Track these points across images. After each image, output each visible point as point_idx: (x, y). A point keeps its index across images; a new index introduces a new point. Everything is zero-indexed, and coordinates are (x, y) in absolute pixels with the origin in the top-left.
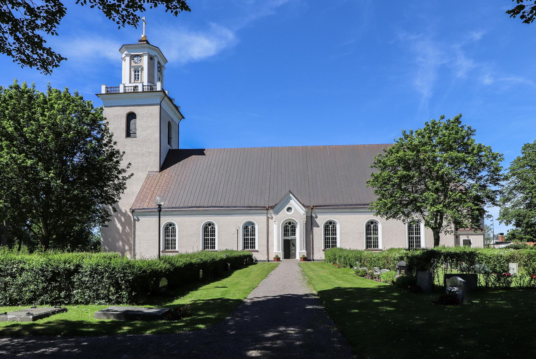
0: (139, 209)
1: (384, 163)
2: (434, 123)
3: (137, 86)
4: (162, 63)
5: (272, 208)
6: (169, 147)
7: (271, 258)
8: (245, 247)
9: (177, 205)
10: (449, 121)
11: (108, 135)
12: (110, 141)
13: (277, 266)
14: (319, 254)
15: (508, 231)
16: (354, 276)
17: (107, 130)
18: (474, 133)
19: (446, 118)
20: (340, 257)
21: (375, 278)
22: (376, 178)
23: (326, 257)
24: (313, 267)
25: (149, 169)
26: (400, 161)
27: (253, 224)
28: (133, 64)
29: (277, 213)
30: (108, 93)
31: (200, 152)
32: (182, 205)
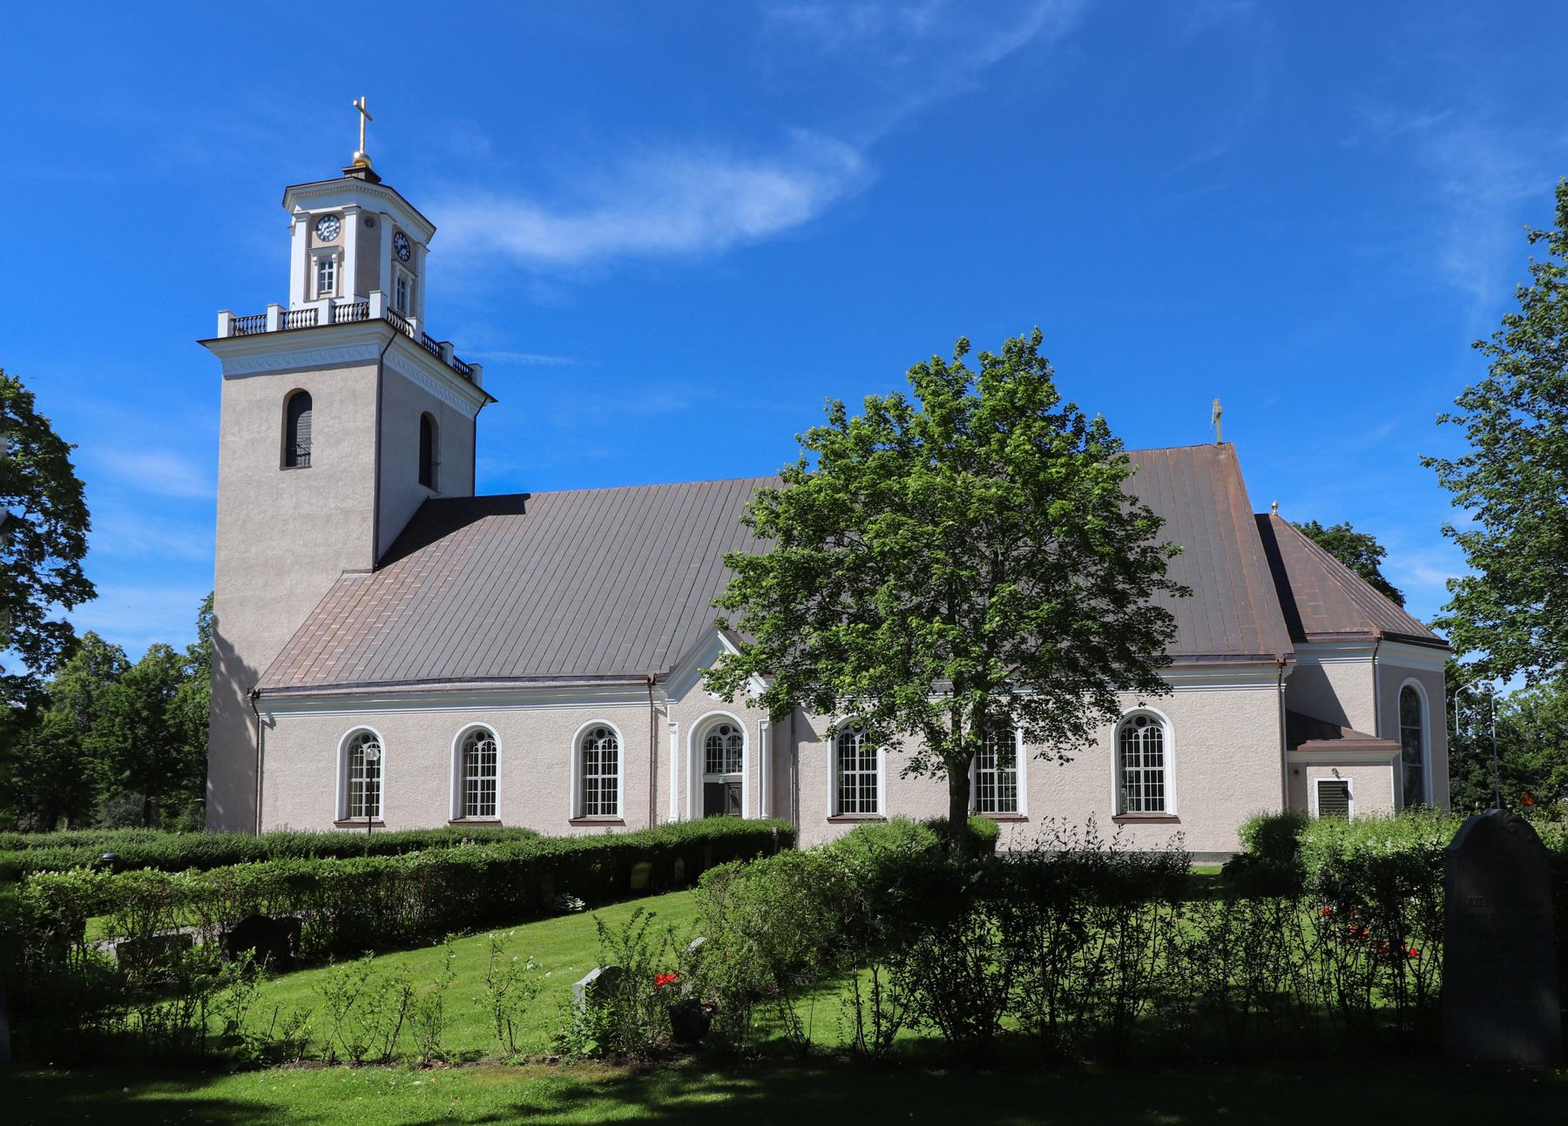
0: (272, 690)
4: (414, 233)
28: (317, 243)
29: (678, 695)
32: (400, 676)
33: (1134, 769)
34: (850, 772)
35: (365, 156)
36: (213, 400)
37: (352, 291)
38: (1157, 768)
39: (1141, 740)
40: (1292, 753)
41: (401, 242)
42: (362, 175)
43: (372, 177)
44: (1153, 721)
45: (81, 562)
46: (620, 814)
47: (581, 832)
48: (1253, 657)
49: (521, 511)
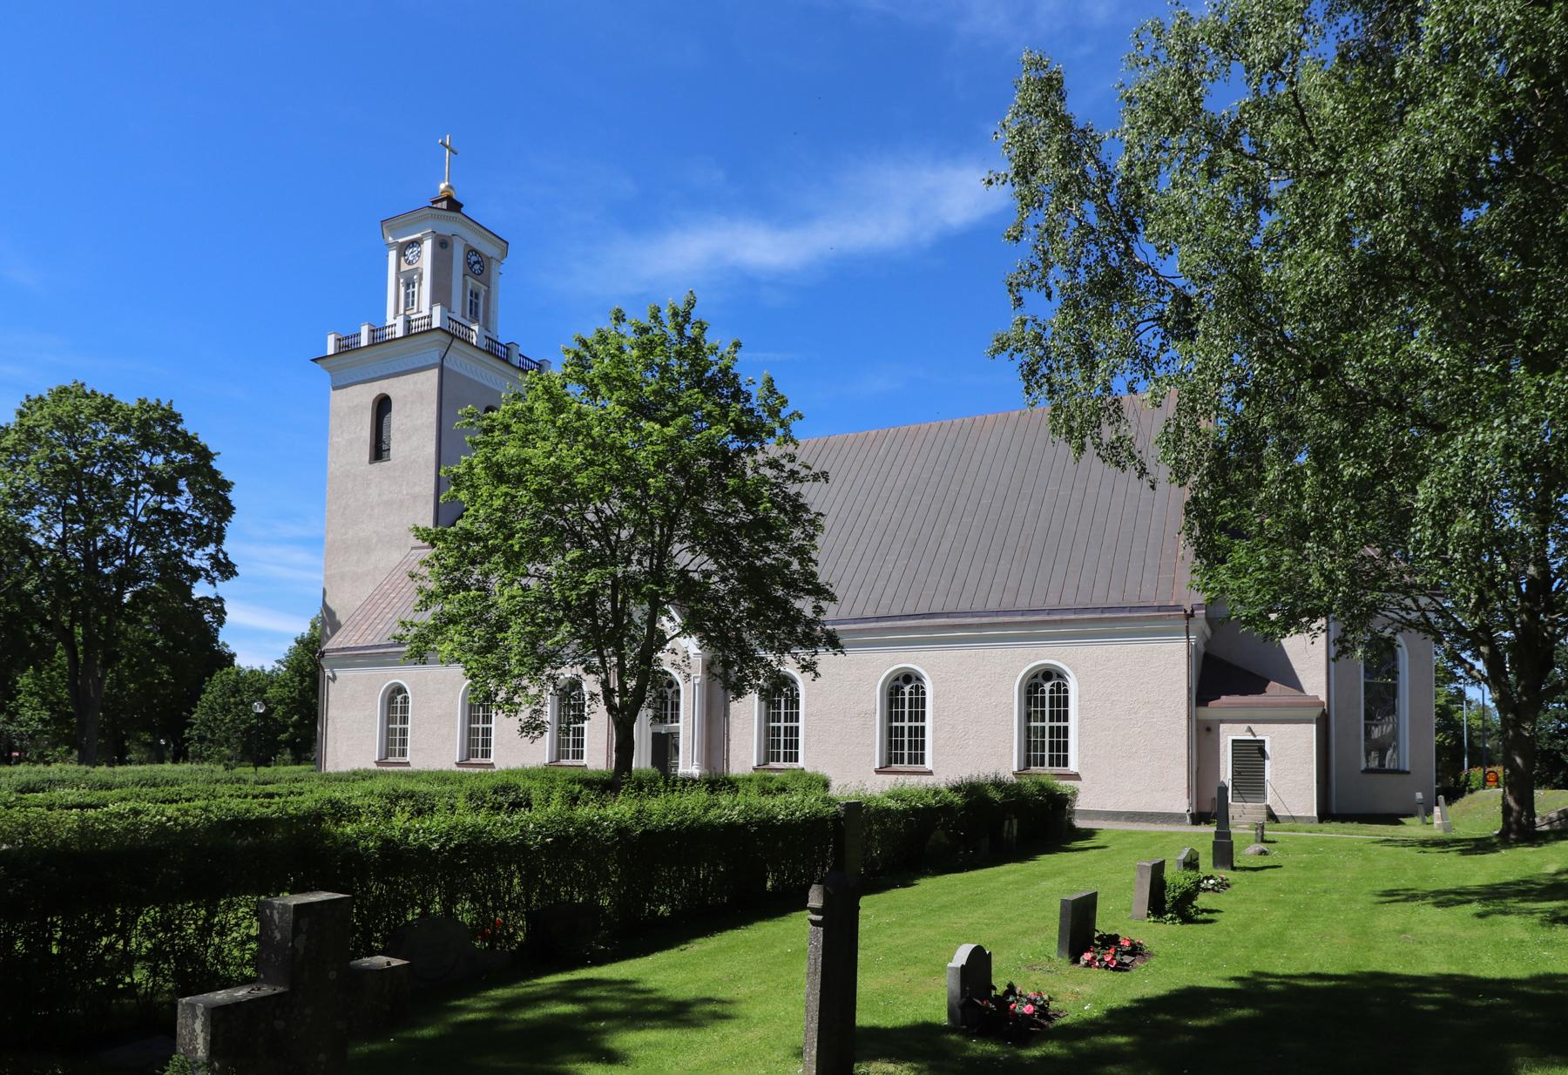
4: (488, 249)
28: (405, 267)
33: (1039, 724)
34: (899, 724)
35: (450, 187)
36: (324, 409)
38: (1062, 724)
39: (1047, 695)
40: (1202, 709)
41: (474, 259)
42: (444, 205)
43: (454, 206)
45: (224, 548)
46: (929, 764)
48: (1159, 608)
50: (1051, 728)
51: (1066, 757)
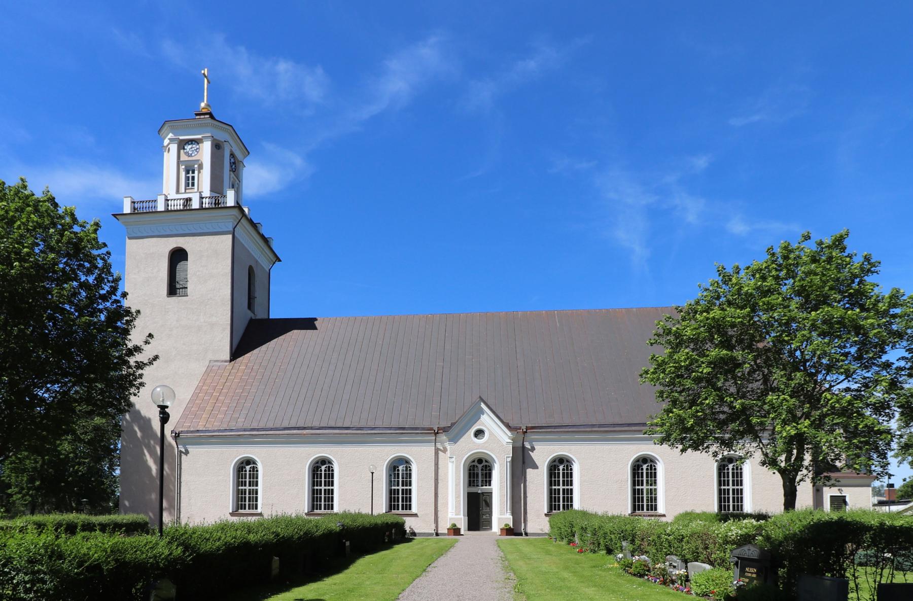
0: (188, 432)
1: (678, 335)
2: (787, 249)
3: (190, 199)
4: (238, 154)
5: (445, 430)
6: (250, 314)
7: (443, 529)
8: (392, 506)
9: (262, 425)
10: (821, 243)
11: (110, 278)
12: (114, 290)
13: (452, 546)
14: (538, 520)
15: (904, 480)
16: (619, 576)
17: (107, 268)
18: (877, 269)
19: (815, 237)
20: (584, 529)
21: (673, 582)
22: (661, 366)
23: (552, 527)
24: (527, 549)
25: (210, 356)
26: (717, 327)
27: (407, 462)
28: (184, 157)
29: (454, 440)
30: (135, 212)
31: (308, 324)
32: (270, 425)
34: (557, 487)
37: (209, 188)
38: (569, 487)
44: (652, 461)
47: (235, 519)
49: (315, 328)
50: (564, 490)
51: (410, 505)
